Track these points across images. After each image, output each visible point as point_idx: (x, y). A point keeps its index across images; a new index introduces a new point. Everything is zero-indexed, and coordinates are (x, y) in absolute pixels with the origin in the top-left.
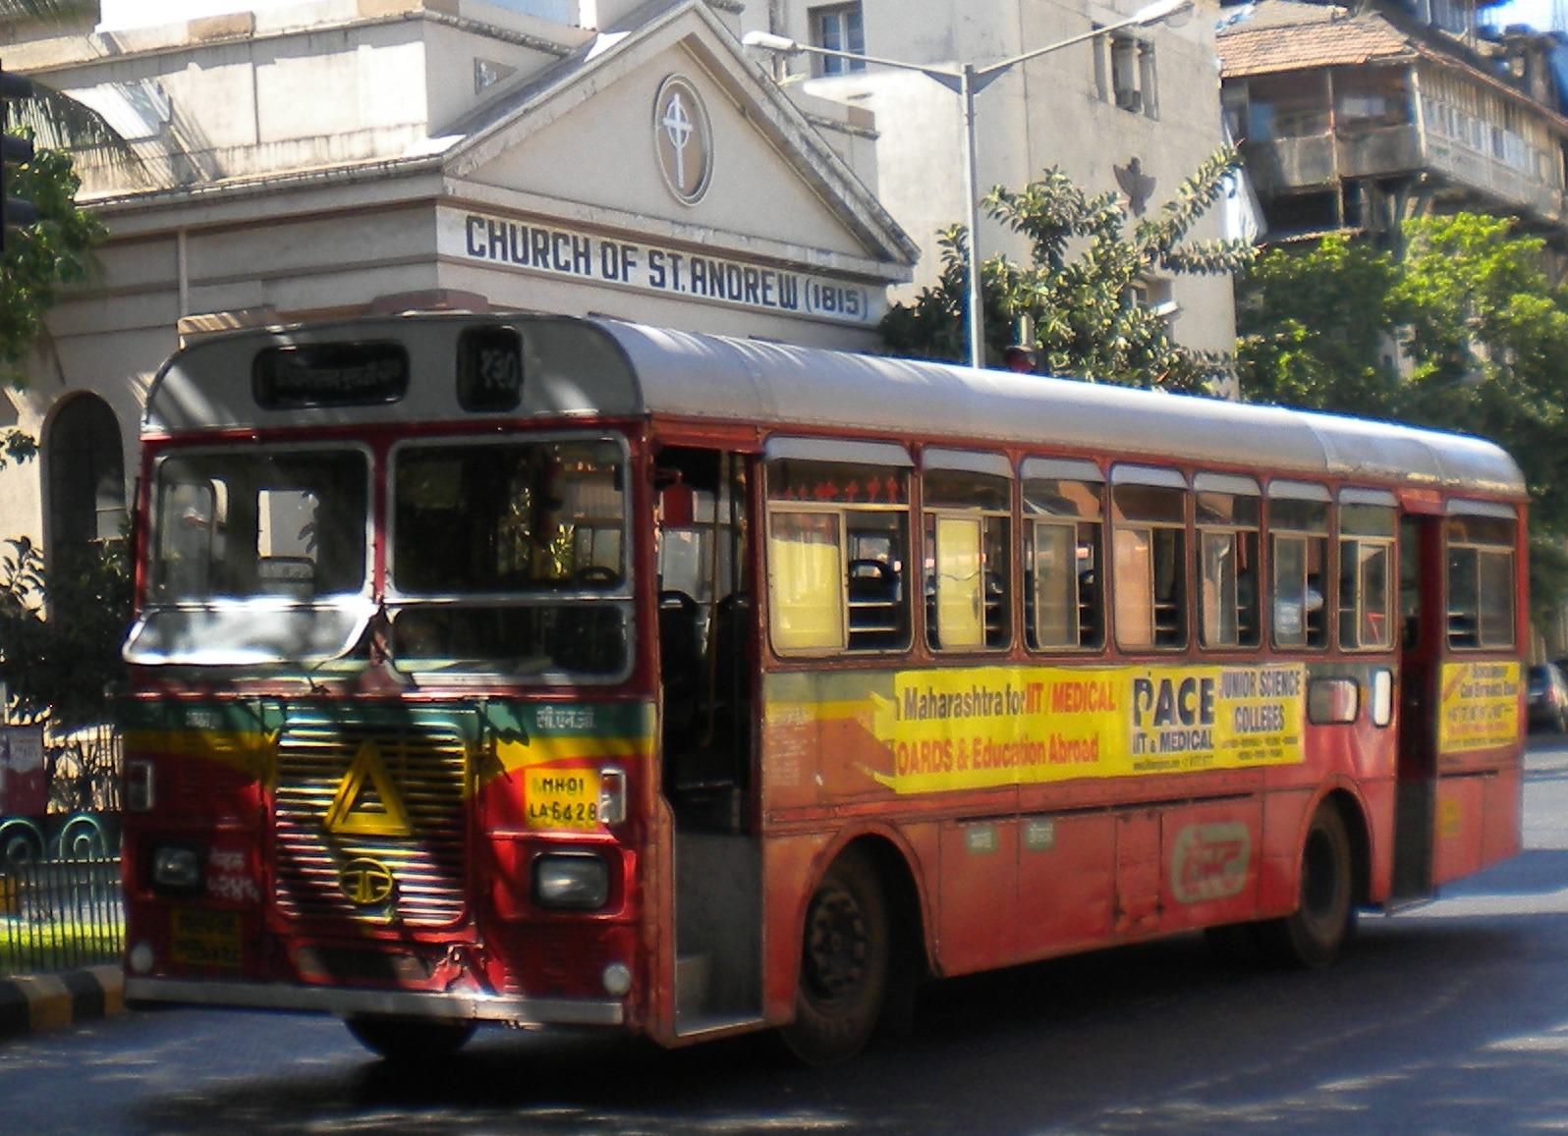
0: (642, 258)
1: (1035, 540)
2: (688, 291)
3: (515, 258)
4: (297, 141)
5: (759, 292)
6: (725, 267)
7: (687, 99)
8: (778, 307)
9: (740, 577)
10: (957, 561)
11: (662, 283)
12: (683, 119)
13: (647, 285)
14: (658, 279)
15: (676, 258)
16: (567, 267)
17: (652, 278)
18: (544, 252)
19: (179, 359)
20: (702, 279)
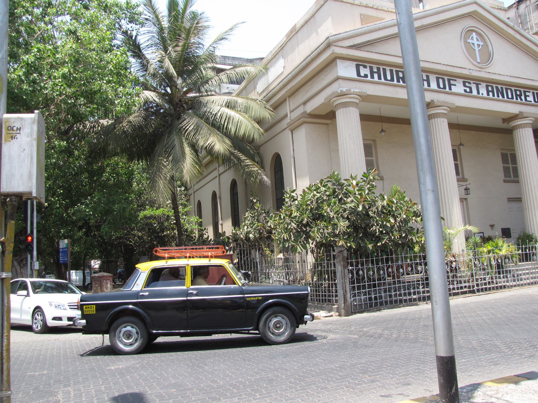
0: (459, 83)
1: (35, 253)
2: (485, 95)
3: (386, 79)
4: (372, 8)
5: (523, 97)
6: (504, 89)
7: (478, 34)
8: (533, 102)
9: (234, 336)
10: (21, 316)
11: (471, 92)
12: (477, 40)
13: (463, 92)
14: (468, 90)
15: (477, 85)
16: (366, 76)
17: (465, 91)
18: (520, 96)
19: (308, 294)
20: (493, 92)
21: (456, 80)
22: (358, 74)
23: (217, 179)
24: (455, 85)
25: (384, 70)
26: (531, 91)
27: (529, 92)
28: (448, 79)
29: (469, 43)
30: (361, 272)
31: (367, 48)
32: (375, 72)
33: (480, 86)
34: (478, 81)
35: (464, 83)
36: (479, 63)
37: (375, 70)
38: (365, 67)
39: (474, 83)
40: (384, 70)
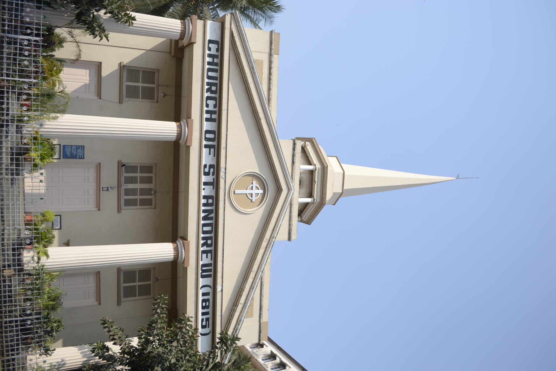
21: (214, 156)
22: (210, 42)
23: (79, 44)
24: (210, 154)
25: (210, 270)
26: (212, 262)
27: (211, 260)
28: (212, 223)
29: (252, 183)
30: (29, 31)
31: (233, 63)
32: (207, 201)
33: (212, 187)
34: (215, 184)
35: (211, 166)
36: (234, 192)
37: (215, 60)
38: (215, 106)
39: (214, 179)
40: (210, 270)
